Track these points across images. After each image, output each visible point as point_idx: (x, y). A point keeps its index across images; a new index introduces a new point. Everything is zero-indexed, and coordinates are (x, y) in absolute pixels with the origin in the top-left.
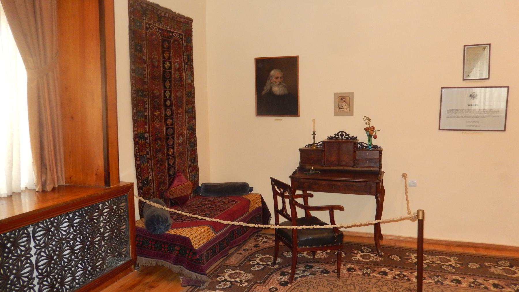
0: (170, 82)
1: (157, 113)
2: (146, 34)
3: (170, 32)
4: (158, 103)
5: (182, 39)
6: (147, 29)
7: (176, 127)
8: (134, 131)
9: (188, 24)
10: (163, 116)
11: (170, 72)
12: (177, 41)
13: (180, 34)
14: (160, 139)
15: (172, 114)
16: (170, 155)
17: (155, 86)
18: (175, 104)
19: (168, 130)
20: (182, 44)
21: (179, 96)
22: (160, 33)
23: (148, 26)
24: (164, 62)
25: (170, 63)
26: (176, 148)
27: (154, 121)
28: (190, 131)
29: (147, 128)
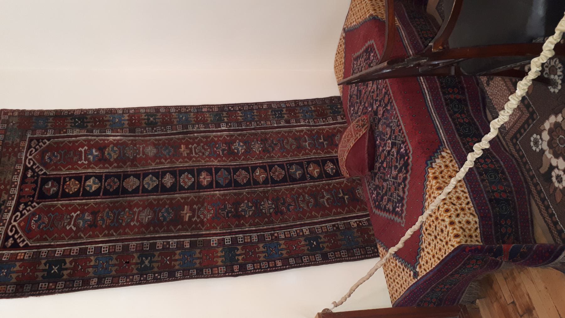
0: (127, 176)
1: (186, 214)
2: (26, 247)
3: (24, 176)
4: (167, 211)
5: (38, 140)
6: (15, 246)
7: (216, 163)
8: (218, 276)
9: (7, 122)
10: (192, 195)
11: (108, 176)
12: (43, 153)
13: (29, 147)
14: (237, 204)
15: (191, 171)
16: (267, 179)
17: (133, 220)
18: (172, 162)
19: (221, 181)
20: (49, 139)
21: (155, 151)
22: (26, 205)
23: (11, 241)
24: (87, 194)
25: (88, 177)
26: (254, 162)
27: (202, 222)
28: (223, 121)
29: (214, 240)
